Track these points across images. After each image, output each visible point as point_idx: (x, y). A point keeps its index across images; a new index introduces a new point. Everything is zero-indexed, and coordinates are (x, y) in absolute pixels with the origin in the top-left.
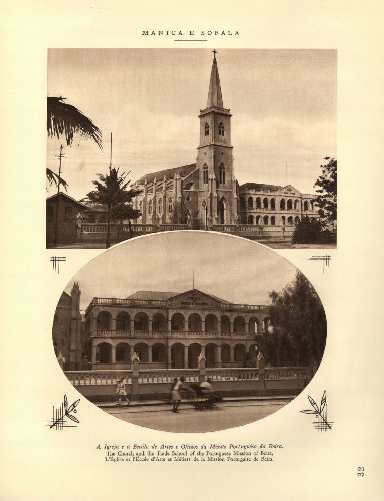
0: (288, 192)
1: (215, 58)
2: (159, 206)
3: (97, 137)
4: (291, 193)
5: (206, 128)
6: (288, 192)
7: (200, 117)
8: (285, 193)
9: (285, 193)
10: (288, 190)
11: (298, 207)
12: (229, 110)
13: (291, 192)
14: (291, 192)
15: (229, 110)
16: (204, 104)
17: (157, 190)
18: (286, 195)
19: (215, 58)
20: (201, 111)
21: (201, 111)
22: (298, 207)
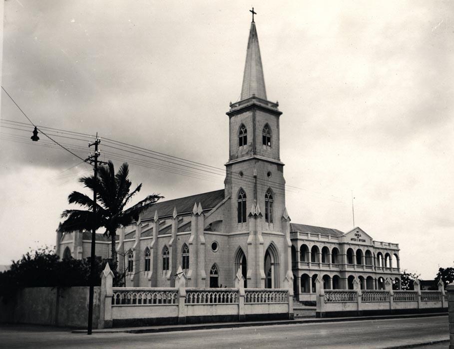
0: (356, 237)
1: (253, 21)
2: (129, 261)
3: (18, 125)
4: (360, 240)
5: (241, 133)
6: (356, 237)
7: (230, 114)
8: (352, 239)
9: (352, 239)
10: (356, 235)
11: (320, 285)
12: (277, 105)
13: (360, 238)
14: (360, 238)
15: (277, 105)
16: (281, 117)
17: (179, 230)
18: (353, 242)
19: (253, 21)
20: (232, 106)
21: (232, 106)
22: (320, 285)
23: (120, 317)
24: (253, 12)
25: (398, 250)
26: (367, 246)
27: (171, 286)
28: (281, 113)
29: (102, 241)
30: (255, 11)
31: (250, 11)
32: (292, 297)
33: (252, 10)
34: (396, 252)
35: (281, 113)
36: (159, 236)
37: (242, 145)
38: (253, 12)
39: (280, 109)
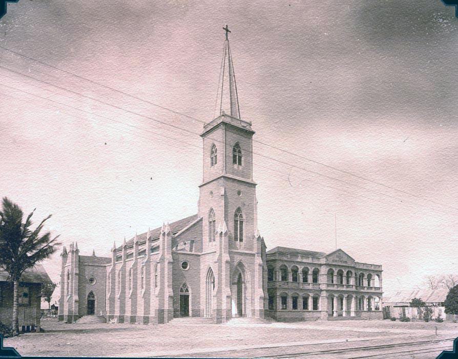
1: (94, 253)
5: (212, 152)
10: (337, 257)
23: (80, 353)
24: (227, 31)
25: (381, 271)
26: (348, 267)
27: (190, 251)
28: (253, 133)
29: (13, 356)
30: (225, 31)
31: (224, 28)
32: (325, 276)
33: (225, 27)
34: (379, 273)
35: (253, 133)
36: (127, 260)
37: (213, 165)
38: (227, 31)
39: (253, 128)
